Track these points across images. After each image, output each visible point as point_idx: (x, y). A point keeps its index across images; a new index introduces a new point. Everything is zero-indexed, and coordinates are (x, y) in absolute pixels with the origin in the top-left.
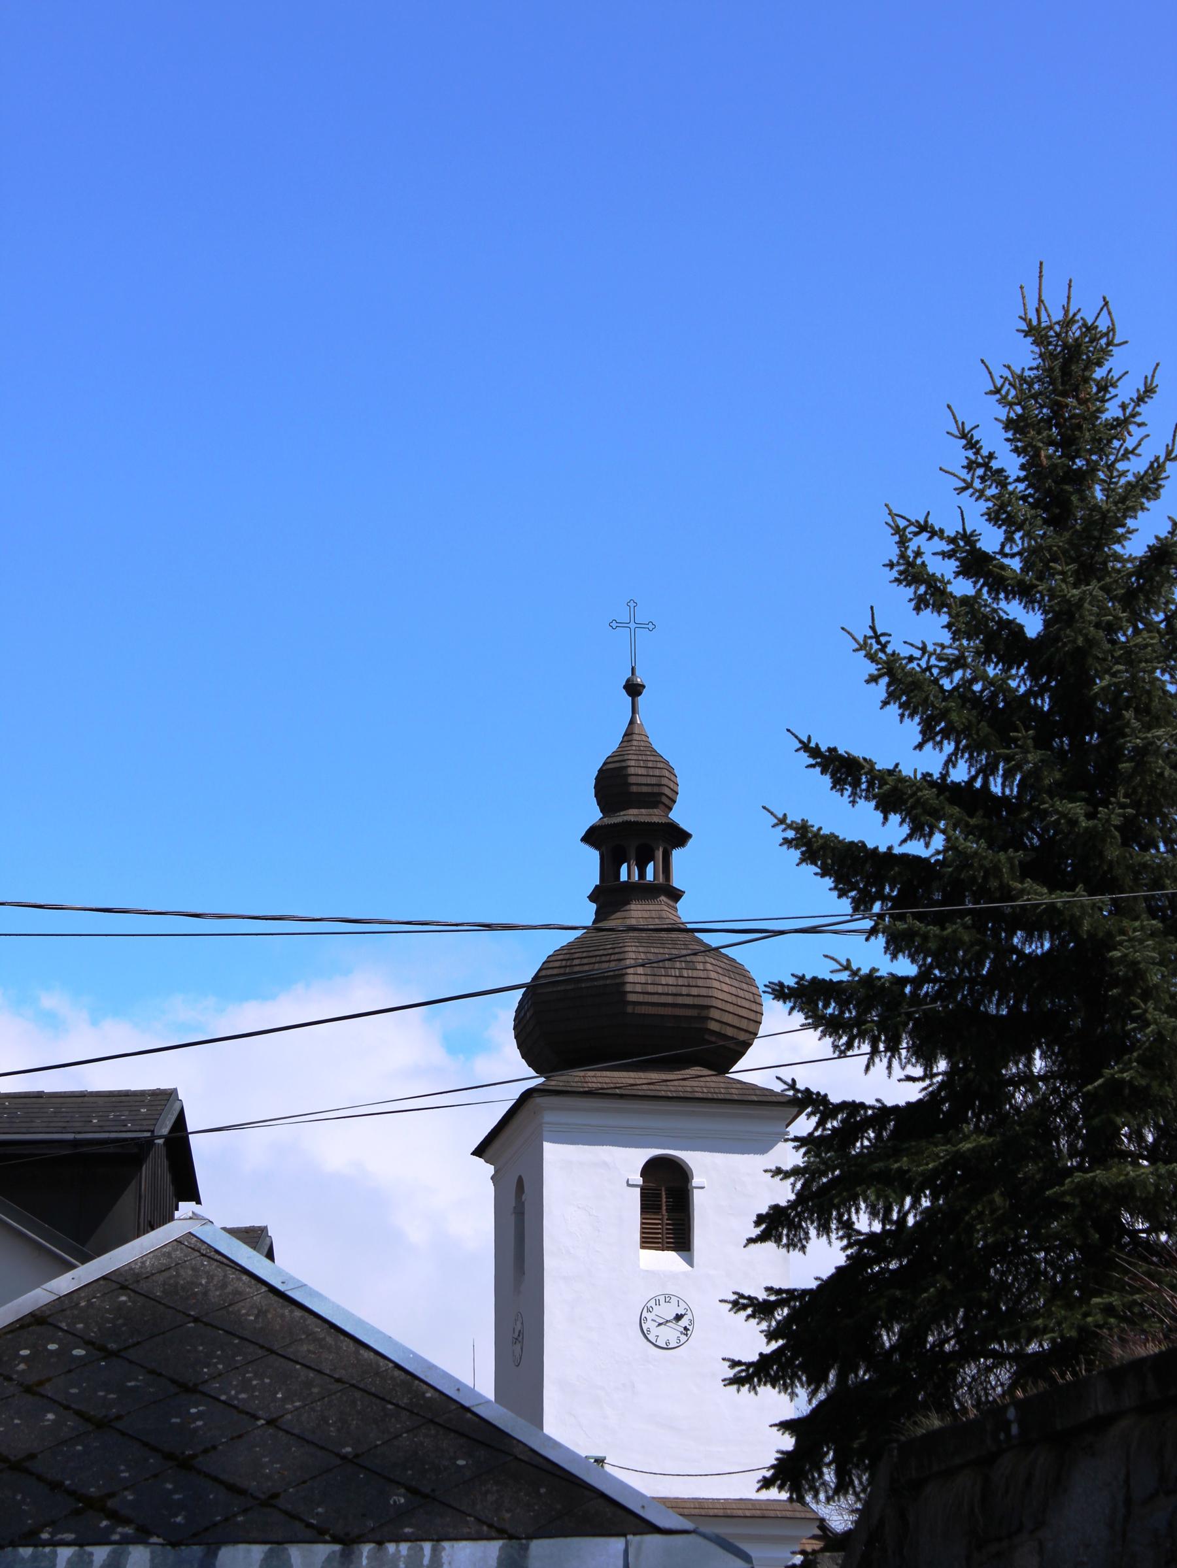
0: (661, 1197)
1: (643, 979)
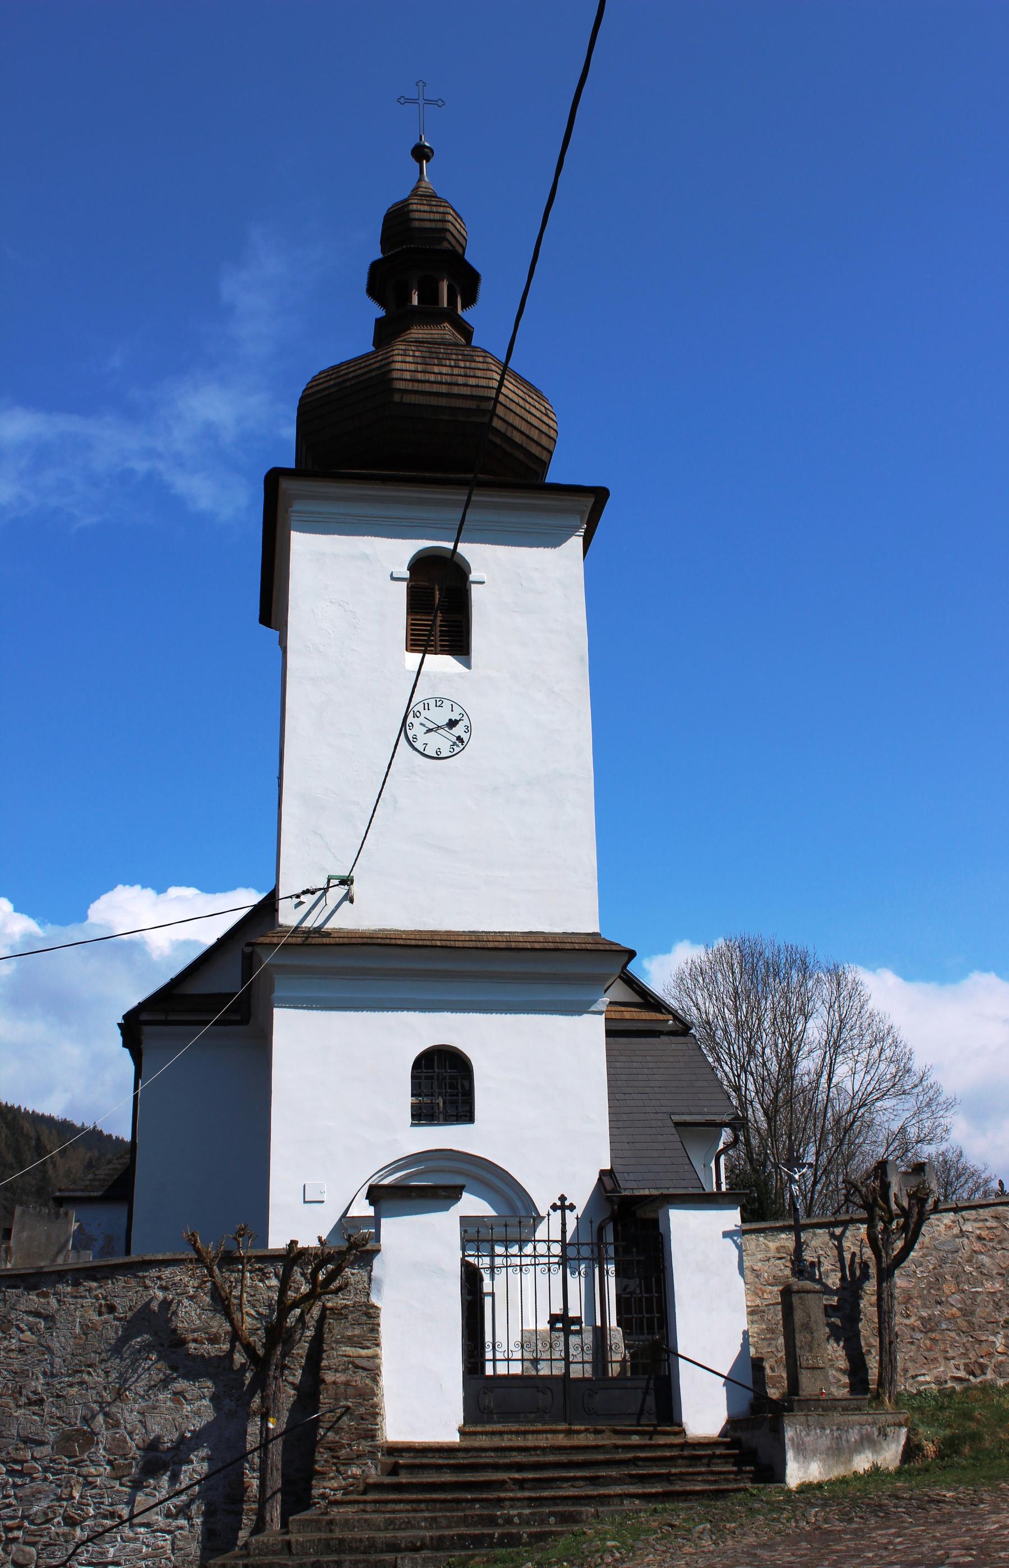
1: (412, 367)
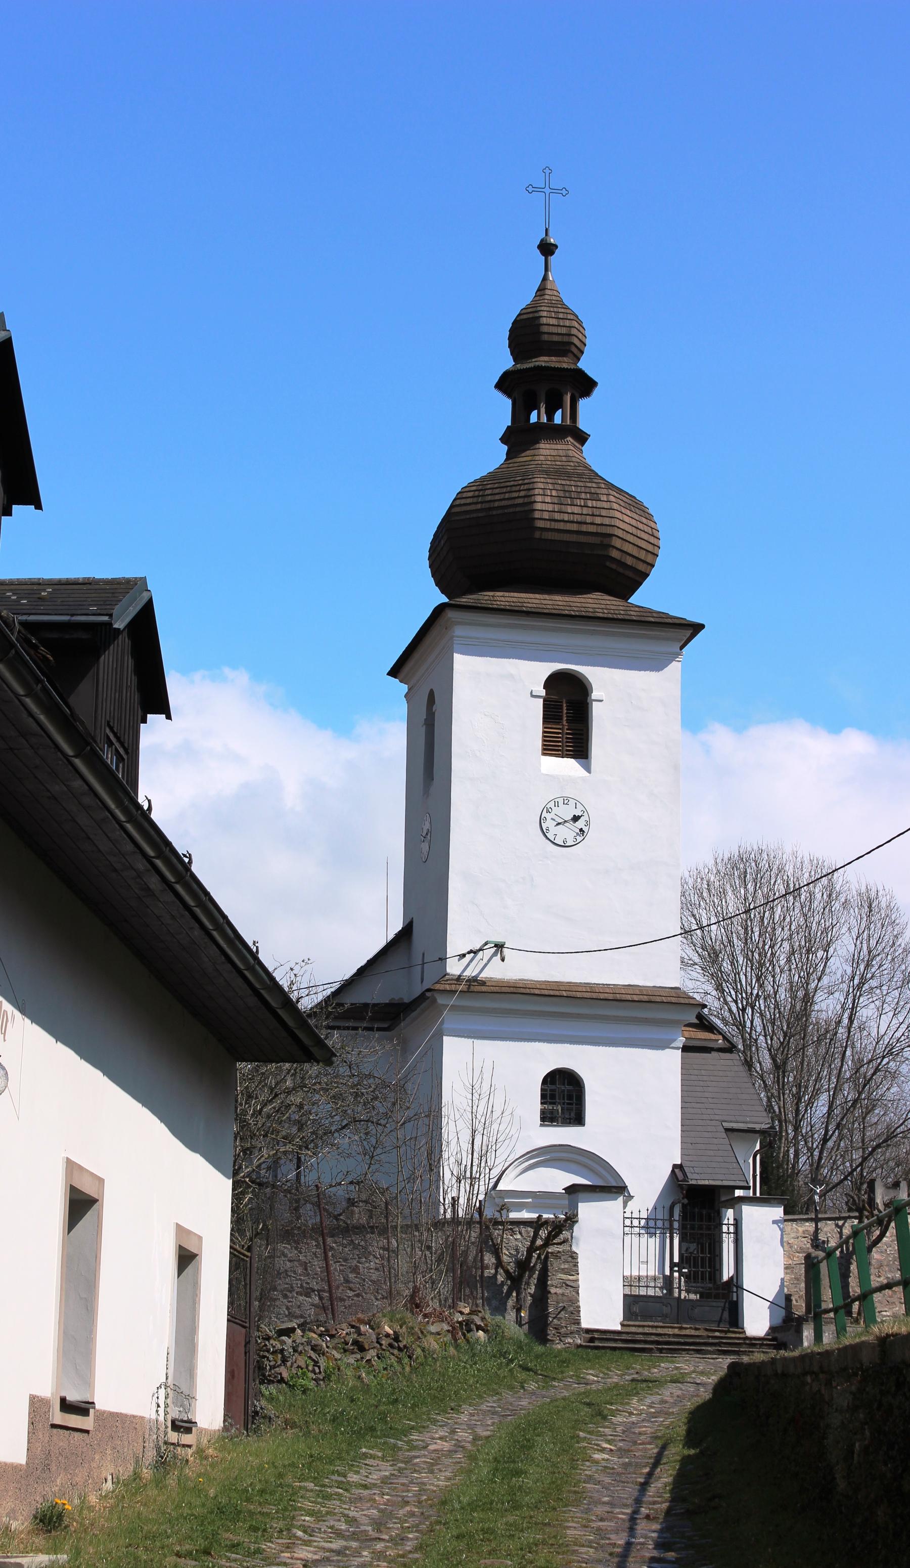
0: (562, 709)
1: (550, 507)
